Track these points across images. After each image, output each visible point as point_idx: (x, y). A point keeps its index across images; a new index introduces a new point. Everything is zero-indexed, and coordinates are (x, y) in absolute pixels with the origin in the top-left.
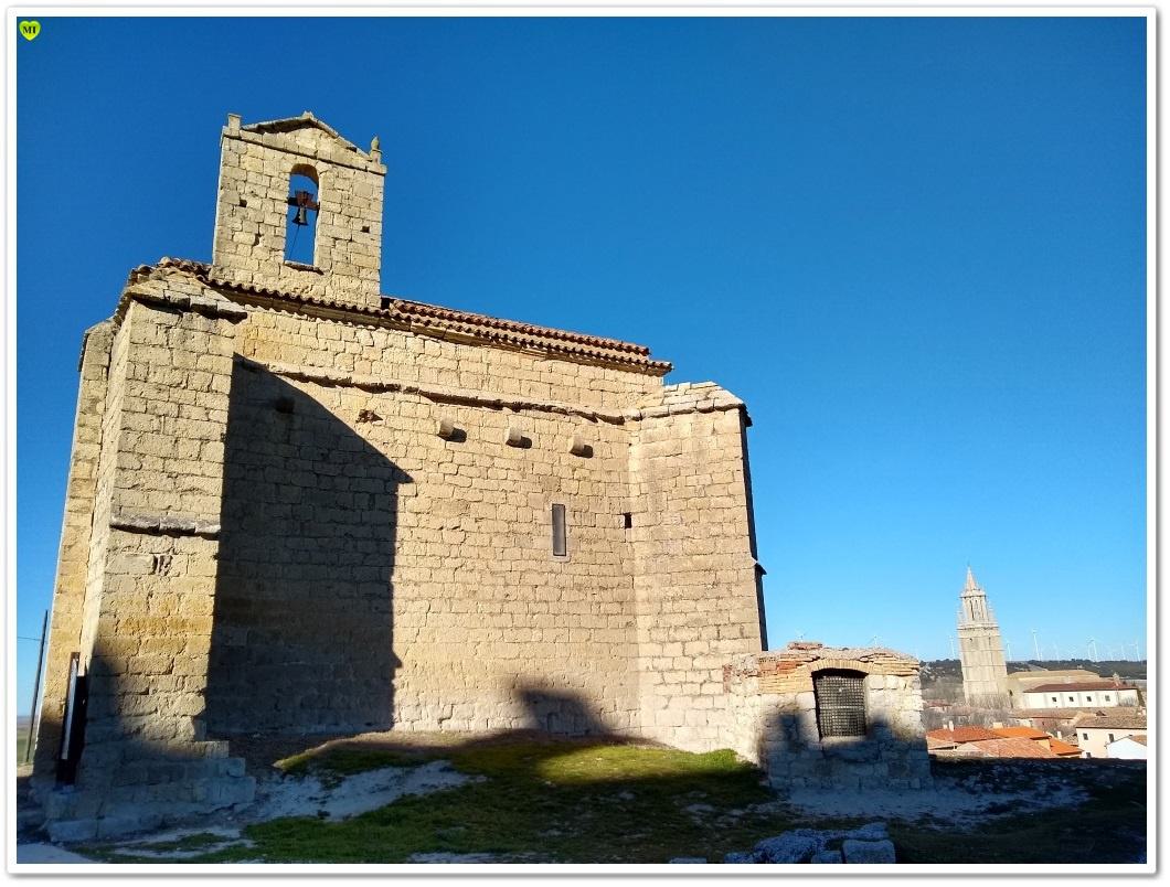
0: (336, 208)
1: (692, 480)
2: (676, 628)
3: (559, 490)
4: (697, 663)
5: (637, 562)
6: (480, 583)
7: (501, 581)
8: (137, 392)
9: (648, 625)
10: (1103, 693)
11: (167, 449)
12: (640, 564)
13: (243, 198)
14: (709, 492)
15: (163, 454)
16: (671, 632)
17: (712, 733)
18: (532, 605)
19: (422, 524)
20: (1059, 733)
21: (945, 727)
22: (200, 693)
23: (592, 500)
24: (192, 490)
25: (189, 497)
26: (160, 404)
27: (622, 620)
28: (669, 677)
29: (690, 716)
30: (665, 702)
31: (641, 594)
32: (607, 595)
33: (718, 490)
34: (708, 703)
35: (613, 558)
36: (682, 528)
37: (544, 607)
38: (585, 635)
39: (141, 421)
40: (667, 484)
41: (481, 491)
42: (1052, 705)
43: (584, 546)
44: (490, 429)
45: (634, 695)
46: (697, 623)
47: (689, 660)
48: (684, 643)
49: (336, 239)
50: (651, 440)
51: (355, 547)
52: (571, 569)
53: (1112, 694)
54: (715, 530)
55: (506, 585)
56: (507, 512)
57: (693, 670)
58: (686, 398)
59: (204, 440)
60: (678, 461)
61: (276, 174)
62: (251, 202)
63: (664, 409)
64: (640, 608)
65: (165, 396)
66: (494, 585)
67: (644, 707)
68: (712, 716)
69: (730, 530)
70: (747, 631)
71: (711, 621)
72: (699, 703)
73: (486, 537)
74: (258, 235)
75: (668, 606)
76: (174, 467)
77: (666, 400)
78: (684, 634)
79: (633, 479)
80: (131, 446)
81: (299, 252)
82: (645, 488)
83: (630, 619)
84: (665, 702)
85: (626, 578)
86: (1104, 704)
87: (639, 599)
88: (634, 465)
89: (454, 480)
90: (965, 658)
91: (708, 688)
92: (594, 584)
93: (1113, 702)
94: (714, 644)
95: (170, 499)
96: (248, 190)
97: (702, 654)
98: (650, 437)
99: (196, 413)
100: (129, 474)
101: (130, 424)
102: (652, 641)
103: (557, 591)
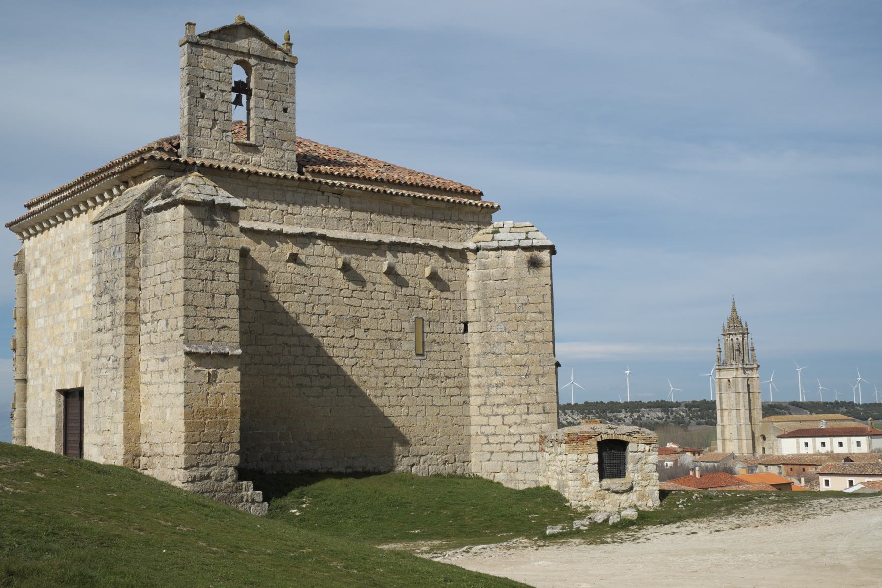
0: (264, 94)
1: (513, 299)
2: (498, 406)
3: (419, 307)
4: (512, 430)
5: (471, 358)
6: (368, 375)
7: (381, 374)
8: (190, 266)
9: (479, 403)
10: (855, 439)
11: (208, 302)
12: (473, 360)
13: (202, 91)
14: (526, 308)
15: (207, 305)
16: (495, 407)
17: (519, 476)
18: (410, 393)
19: (330, 334)
20: (803, 479)
21: (691, 473)
22: (237, 453)
23: (441, 313)
24: (224, 327)
25: (222, 332)
26: (202, 272)
27: (460, 400)
28: (492, 439)
29: (506, 465)
30: (488, 456)
31: (474, 381)
32: (450, 382)
33: (531, 307)
34: (518, 456)
35: (456, 355)
36: (506, 334)
37: (409, 391)
38: (436, 410)
39: (195, 285)
40: (496, 301)
41: (368, 308)
42: (803, 451)
43: (436, 348)
44: (374, 267)
45: (468, 453)
46: (515, 403)
47: (507, 428)
48: (503, 416)
49: (266, 119)
50: (484, 267)
51: (289, 351)
52: (427, 364)
53: (863, 440)
54: (529, 337)
55: (385, 376)
56: (385, 324)
57: (510, 434)
58: (510, 236)
59: (228, 295)
60: (503, 284)
61: (222, 69)
62: (209, 95)
63: (495, 244)
64: (473, 391)
65: (204, 266)
66: (377, 377)
67: (473, 459)
68: (522, 466)
69: (539, 337)
70: (548, 406)
71: (523, 401)
72: (512, 457)
73: (372, 342)
74: (214, 120)
75: (493, 390)
76: (213, 313)
77: (497, 236)
78: (503, 410)
79: (471, 296)
80: (189, 301)
81: (248, 139)
82: (479, 303)
83: (466, 398)
84: (488, 456)
85: (464, 370)
86: (855, 450)
87: (472, 384)
88: (471, 286)
89: (351, 301)
90: (721, 399)
91: (519, 447)
92: (442, 375)
93: (864, 449)
94: (524, 417)
95: (212, 334)
96: (205, 84)
97: (516, 423)
98: (484, 265)
99: (222, 276)
100: (191, 319)
101: (188, 287)
102: (481, 414)
103: (418, 380)
